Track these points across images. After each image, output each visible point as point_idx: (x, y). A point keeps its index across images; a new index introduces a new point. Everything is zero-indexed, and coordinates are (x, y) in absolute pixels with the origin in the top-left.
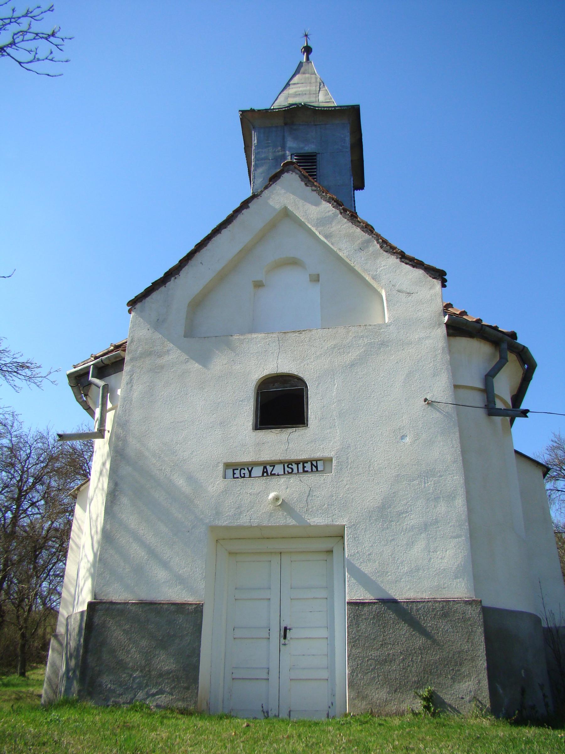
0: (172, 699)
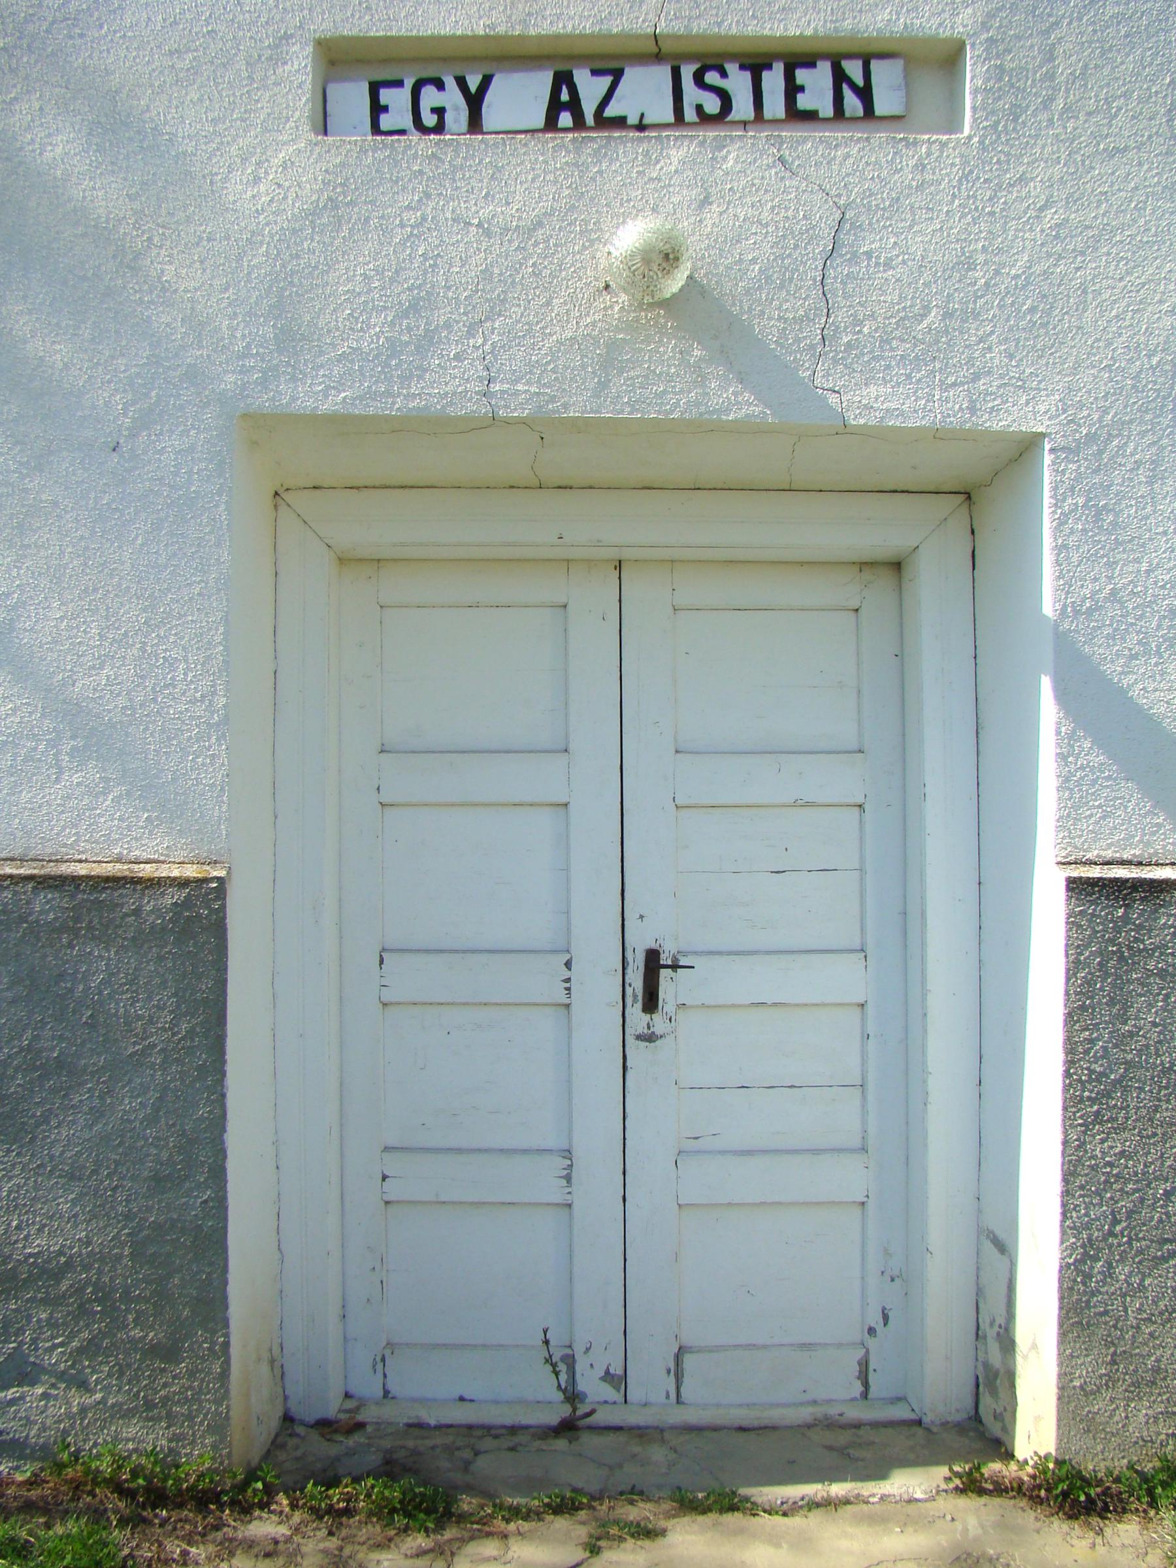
0: (83, 1410)
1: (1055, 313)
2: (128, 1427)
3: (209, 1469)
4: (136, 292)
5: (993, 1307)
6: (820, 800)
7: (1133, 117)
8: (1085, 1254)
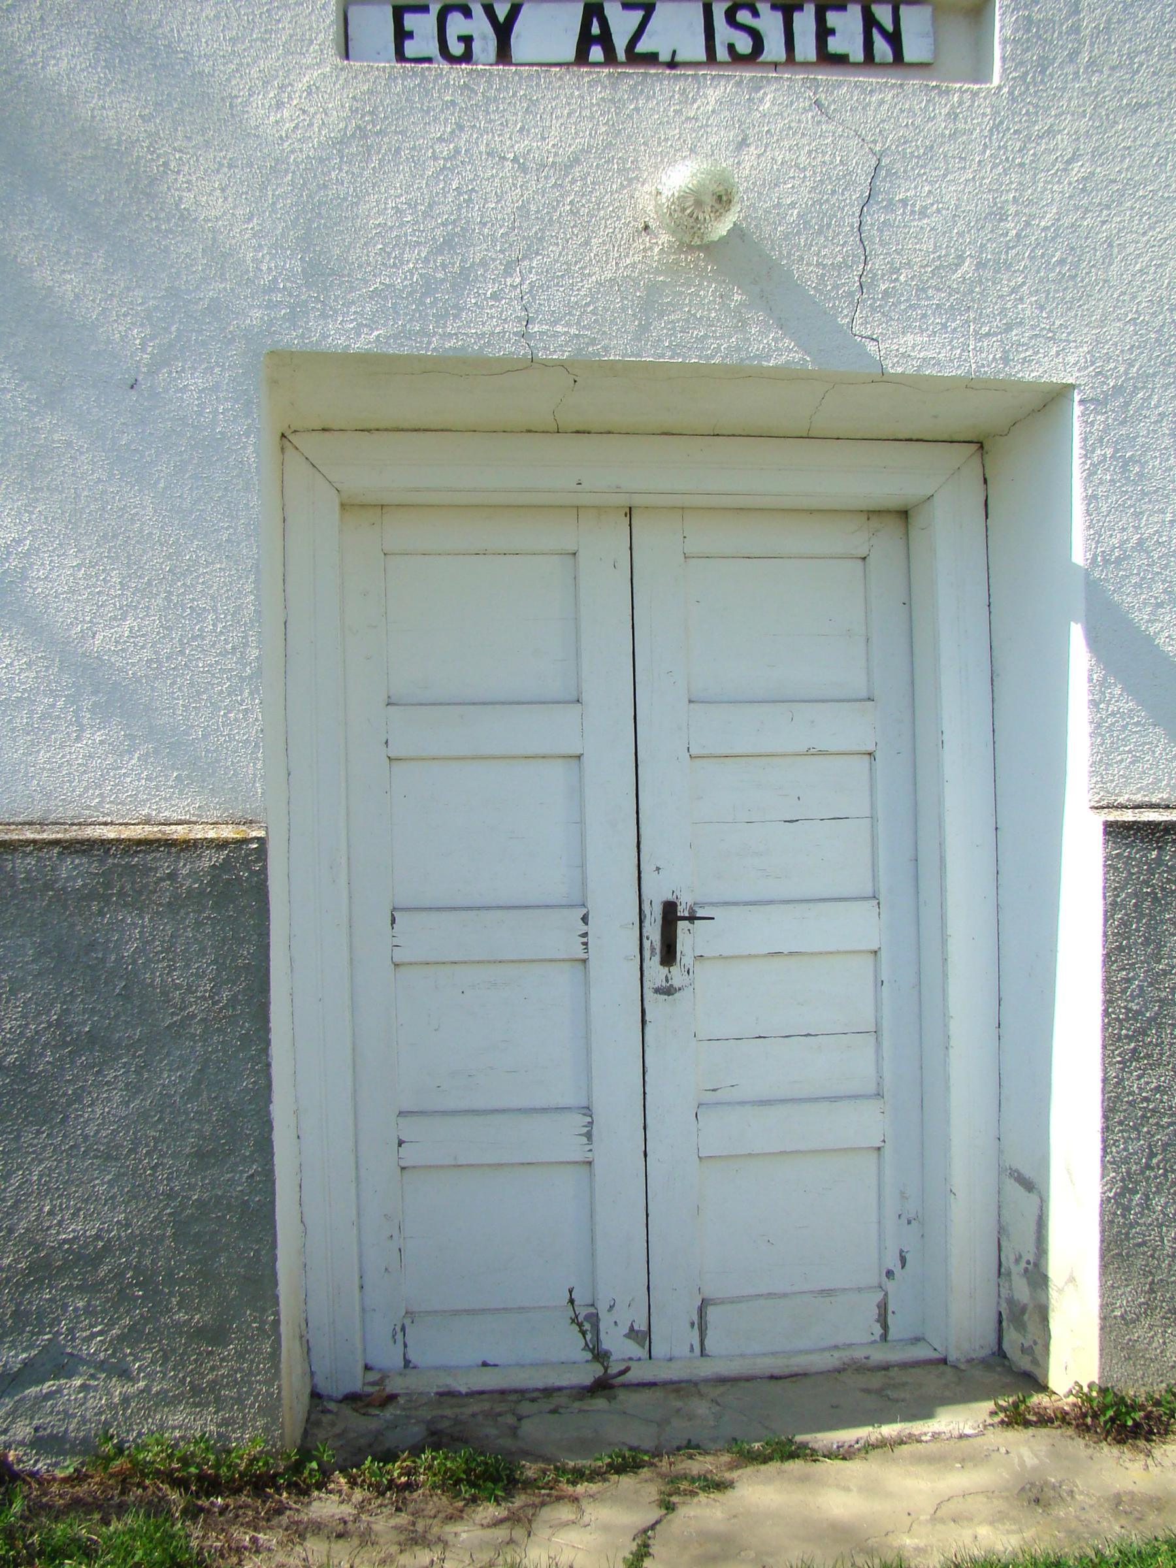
0: (126, 1400)
1: (1082, 266)
2: (174, 1415)
3: (261, 1452)
4: (152, 219)
5: (1021, 1243)
6: (833, 749)
7: (1154, 73)
8: (1124, 1188)
